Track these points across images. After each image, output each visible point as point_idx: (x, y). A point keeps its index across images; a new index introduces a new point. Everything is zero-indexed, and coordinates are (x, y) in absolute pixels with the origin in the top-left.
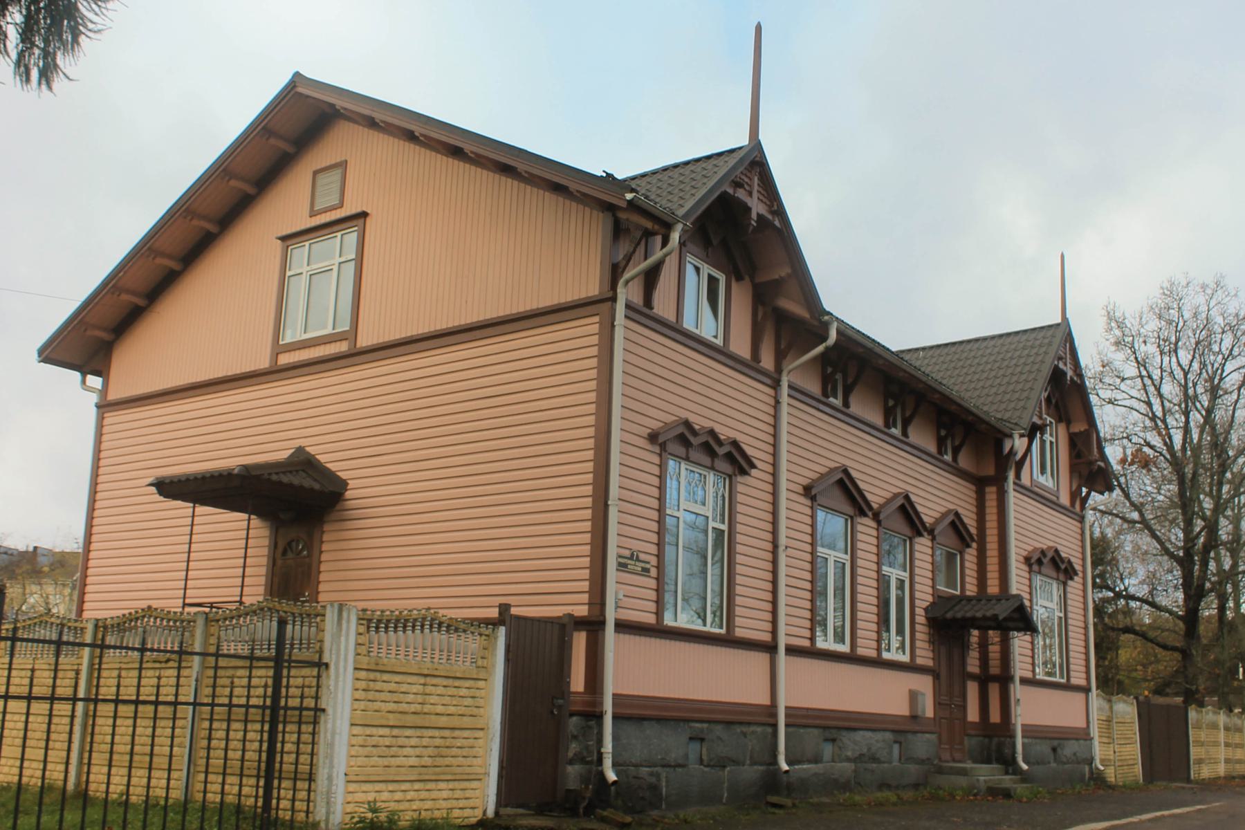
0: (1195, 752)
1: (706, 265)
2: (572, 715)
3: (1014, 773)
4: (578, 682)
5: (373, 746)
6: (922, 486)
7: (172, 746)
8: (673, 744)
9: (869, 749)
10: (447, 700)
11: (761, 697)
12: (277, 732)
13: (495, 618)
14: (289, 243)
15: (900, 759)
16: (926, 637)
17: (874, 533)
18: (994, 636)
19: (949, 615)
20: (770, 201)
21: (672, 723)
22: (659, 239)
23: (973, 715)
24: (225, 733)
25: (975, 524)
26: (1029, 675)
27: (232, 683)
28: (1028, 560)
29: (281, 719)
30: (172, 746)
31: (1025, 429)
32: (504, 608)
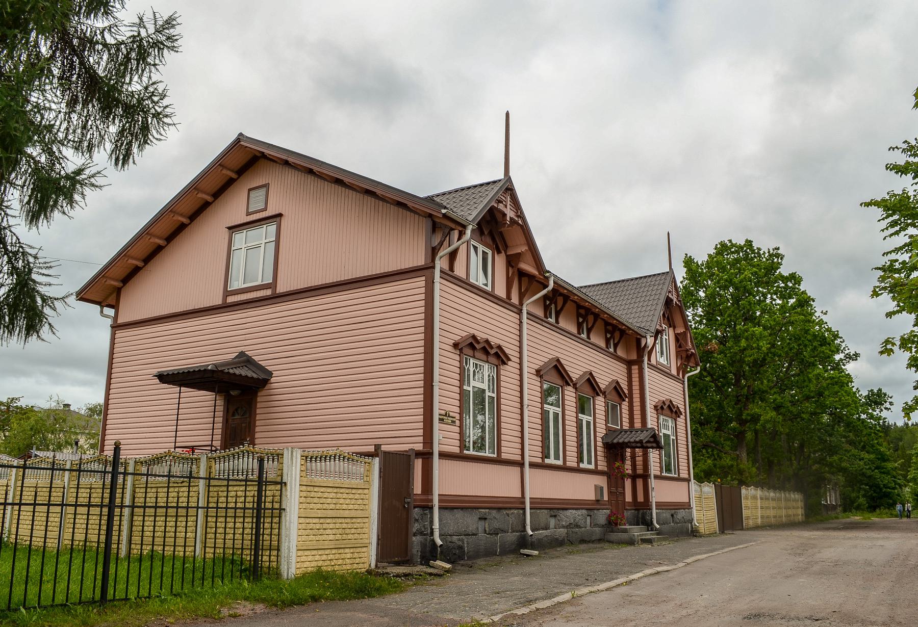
0: (745, 513)
2: (415, 507)
4: (418, 489)
6: (598, 366)
7: (186, 532)
8: (469, 521)
9: (575, 520)
10: (348, 501)
11: (514, 492)
13: (372, 452)
14: (234, 230)
16: (602, 454)
18: (639, 451)
19: (615, 441)
21: (469, 510)
22: (456, 234)
23: (629, 498)
26: (658, 473)
27: (218, 494)
30: (186, 532)
32: (377, 447)
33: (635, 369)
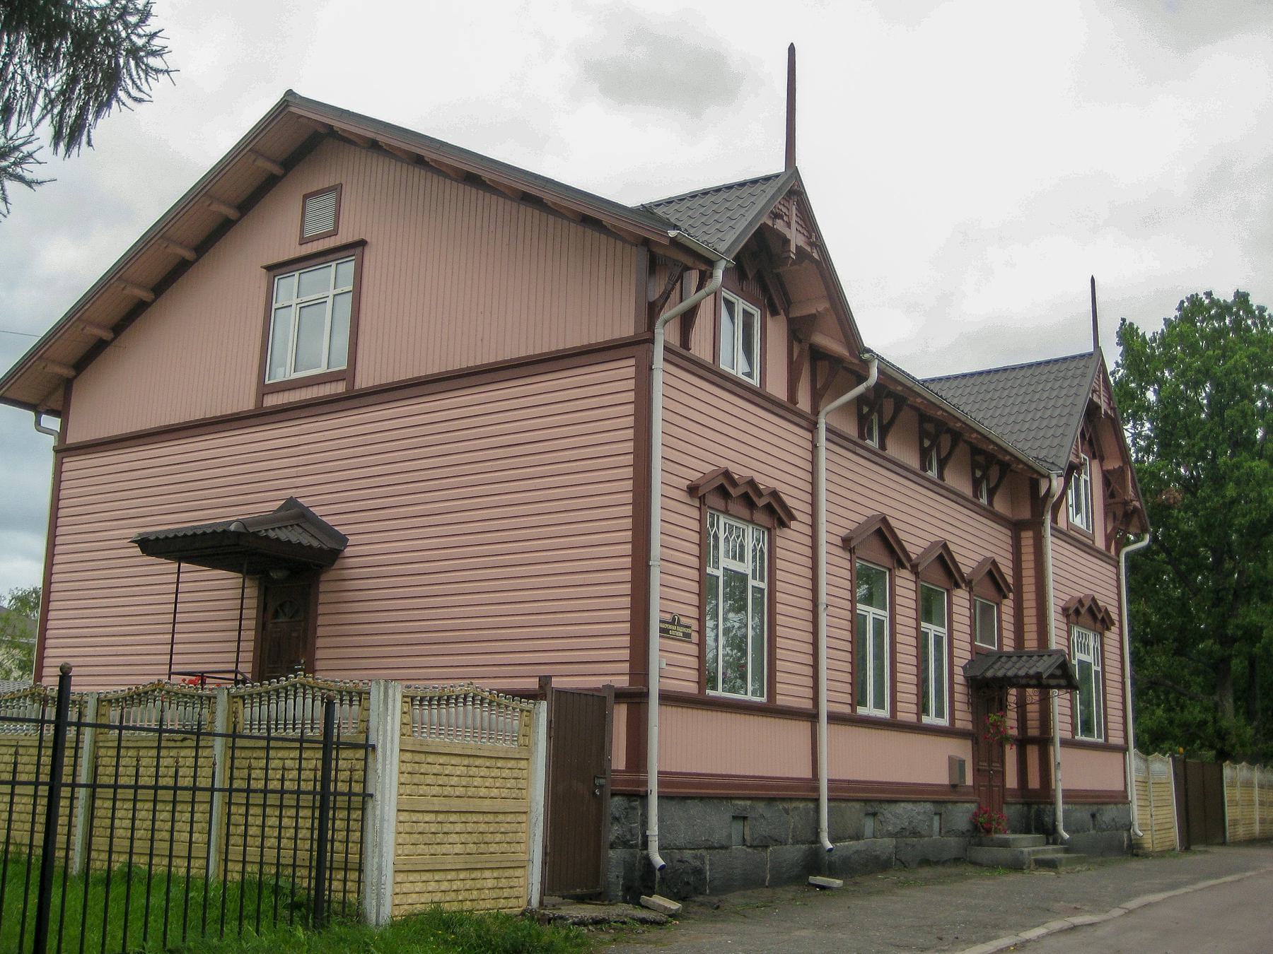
1: (741, 300)
2: (613, 795)
3: (1055, 843)
4: (619, 760)
5: (420, 833)
9: (910, 822)
12: (328, 819)
15: (940, 832)
19: (989, 674)
23: (1011, 781)
26: (1068, 735)
28: (1065, 611)
29: (331, 805)
30: (191, 833)
31: (1063, 469)
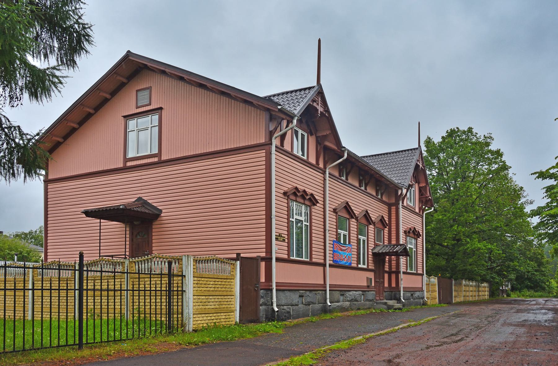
1: (300, 130)
2: (261, 290)
4: (263, 279)
17: (356, 224)
19: (380, 252)
20: (324, 107)
23: (386, 285)
24: (107, 303)
25: (388, 220)
26: (405, 270)
28: (405, 232)
32: (238, 255)
33: (393, 209)
